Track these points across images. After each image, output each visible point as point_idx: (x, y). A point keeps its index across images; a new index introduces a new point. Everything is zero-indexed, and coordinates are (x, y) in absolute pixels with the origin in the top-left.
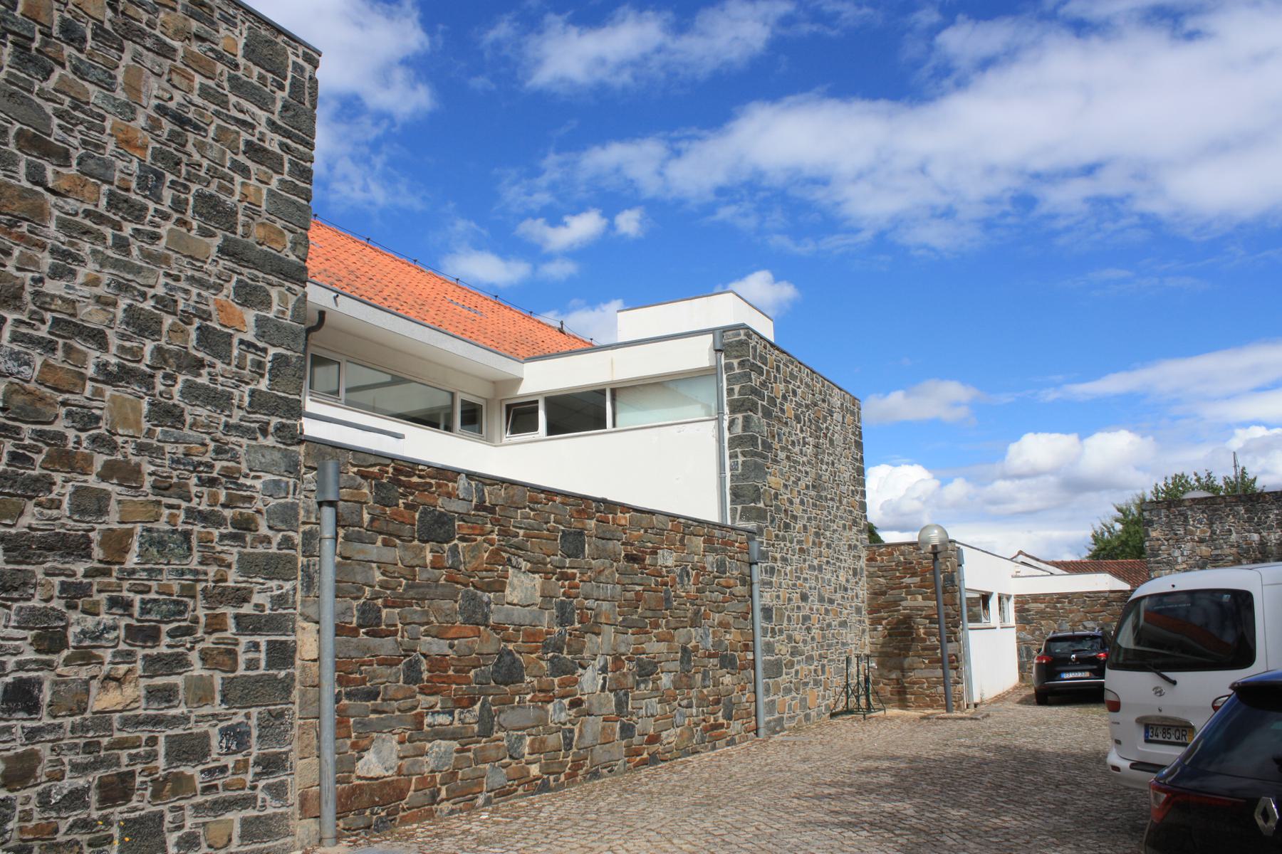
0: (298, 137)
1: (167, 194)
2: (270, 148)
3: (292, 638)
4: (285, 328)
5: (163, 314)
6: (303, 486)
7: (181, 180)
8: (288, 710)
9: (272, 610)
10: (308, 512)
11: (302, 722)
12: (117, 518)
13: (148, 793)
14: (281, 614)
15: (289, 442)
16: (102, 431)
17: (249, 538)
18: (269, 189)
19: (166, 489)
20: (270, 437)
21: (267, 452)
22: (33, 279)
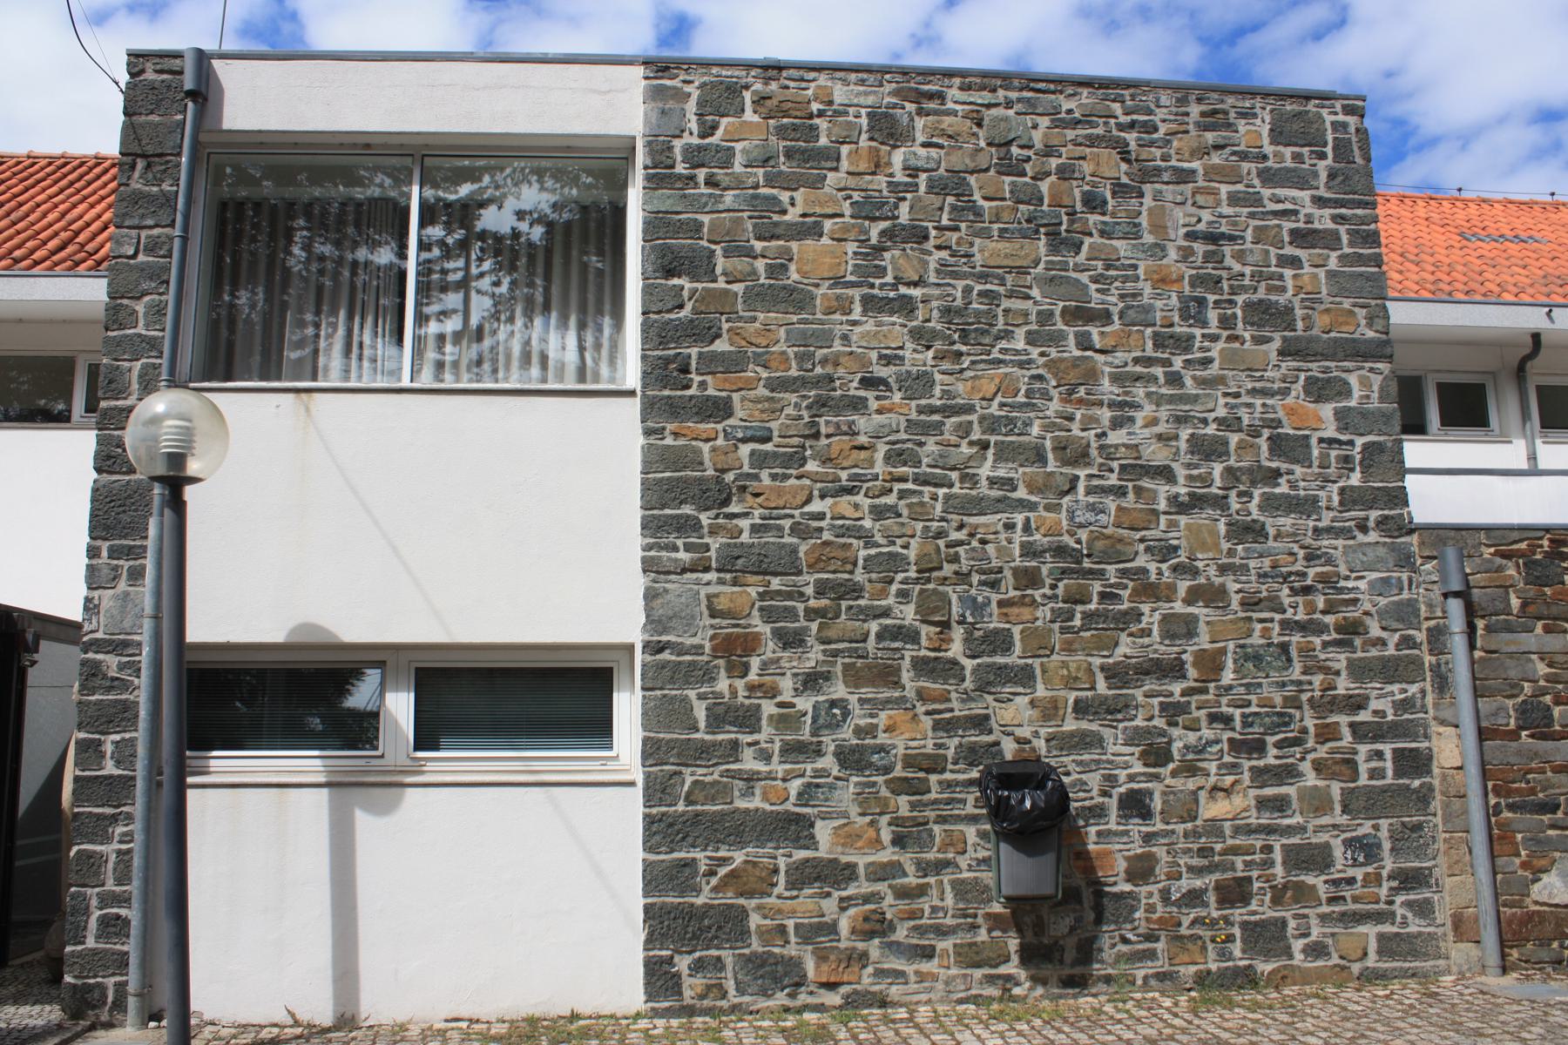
0: (1349, 201)
1: (1213, 316)
2: (1321, 227)
3: (1426, 744)
4: (1373, 413)
5: (1227, 434)
6: (1421, 579)
7: (1226, 297)
8: (1427, 822)
9: (1395, 715)
10: (1430, 606)
11: (1447, 835)
12: (1207, 638)
13: (1268, 898)
14: (1408, 720)
15: (1396, 534)
16: (1183, 559)
17: (1358, 642)
18: (1327, 271)
19: (1256, 604)
20: (1372, 533)
21: (1369, 551)
22: (1096, 435)
